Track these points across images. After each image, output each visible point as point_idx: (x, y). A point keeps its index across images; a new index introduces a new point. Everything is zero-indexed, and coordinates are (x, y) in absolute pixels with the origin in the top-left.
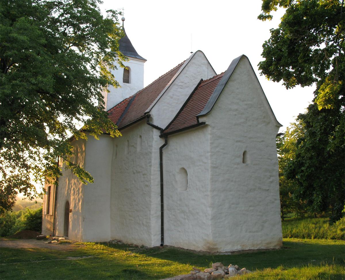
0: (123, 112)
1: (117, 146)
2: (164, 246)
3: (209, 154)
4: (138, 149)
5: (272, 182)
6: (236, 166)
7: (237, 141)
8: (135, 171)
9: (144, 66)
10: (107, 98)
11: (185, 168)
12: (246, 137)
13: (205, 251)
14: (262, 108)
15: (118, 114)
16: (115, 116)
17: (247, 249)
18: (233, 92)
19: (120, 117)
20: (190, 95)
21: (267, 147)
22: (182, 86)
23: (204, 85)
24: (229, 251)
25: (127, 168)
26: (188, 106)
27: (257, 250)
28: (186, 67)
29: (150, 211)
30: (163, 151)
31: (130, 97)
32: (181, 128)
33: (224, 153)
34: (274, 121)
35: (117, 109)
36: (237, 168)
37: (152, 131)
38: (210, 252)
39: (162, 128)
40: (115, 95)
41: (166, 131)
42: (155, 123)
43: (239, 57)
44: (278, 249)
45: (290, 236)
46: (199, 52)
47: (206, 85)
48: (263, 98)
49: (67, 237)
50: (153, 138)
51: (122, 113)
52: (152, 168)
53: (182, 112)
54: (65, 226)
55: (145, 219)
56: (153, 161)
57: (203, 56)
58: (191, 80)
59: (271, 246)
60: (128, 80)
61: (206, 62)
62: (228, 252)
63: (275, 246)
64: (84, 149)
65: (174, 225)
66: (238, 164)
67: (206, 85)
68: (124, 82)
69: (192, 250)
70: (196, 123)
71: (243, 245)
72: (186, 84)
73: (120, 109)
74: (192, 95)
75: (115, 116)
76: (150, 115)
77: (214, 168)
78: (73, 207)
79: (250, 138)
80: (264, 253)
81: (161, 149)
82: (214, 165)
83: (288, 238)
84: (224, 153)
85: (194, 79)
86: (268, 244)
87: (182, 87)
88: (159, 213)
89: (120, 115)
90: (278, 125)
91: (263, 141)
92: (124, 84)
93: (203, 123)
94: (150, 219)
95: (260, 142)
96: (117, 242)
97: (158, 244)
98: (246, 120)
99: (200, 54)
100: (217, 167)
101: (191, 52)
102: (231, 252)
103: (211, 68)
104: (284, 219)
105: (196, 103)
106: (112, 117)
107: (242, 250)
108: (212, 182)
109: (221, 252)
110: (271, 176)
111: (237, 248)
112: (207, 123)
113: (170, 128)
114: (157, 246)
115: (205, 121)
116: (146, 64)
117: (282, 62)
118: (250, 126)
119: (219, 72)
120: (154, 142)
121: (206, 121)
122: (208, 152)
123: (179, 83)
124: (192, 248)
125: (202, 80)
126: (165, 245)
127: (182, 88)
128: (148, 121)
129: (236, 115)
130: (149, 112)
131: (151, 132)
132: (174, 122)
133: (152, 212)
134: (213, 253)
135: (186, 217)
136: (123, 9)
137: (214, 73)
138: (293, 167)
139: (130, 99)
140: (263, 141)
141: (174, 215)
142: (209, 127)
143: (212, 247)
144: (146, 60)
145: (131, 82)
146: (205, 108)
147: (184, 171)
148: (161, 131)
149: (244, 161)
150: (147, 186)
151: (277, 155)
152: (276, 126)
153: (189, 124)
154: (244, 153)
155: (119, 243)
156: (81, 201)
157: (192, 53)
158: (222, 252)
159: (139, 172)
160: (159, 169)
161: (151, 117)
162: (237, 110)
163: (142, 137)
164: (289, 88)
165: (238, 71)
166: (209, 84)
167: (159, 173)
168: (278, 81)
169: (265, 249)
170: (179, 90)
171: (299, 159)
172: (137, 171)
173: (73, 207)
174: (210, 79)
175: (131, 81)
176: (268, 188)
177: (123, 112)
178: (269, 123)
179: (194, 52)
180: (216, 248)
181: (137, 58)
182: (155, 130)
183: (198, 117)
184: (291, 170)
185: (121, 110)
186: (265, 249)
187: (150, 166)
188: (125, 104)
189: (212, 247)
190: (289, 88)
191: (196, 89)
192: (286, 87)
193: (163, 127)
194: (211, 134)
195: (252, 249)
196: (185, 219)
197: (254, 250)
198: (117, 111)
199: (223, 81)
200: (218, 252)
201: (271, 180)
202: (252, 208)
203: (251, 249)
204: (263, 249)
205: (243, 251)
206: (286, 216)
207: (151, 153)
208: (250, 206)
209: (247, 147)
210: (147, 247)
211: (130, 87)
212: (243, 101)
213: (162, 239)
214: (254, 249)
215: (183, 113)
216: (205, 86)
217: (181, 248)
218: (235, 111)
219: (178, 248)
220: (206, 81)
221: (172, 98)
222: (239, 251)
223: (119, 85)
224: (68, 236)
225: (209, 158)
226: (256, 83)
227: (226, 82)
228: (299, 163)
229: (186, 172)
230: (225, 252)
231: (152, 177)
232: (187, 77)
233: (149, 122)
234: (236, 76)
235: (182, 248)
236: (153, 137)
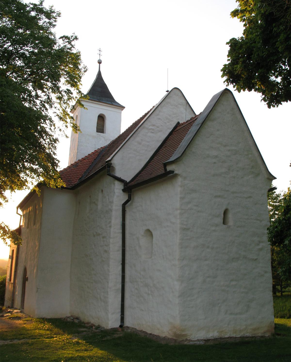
0: (91, 164)
1: (79, 203)
2: (124, 327)
3: (179, 211)
4: (100, 207)
5: (261, 250)
6: (213, 228)
7: (216, 197)
8: (95, 234)
9: (122, 114)
10: (78, 150)
11: (151, 230)
12: (228, 191)
13: (171, 338)
14: (250, 156)
15: (85, 167)
16: (81, 168)
17: (226, 336)
18: (212, 135)
19: (87, 170)
20: (163, 140)
21: (256, 204)
22: (153, 129)
23: (180, 129)
24: (202, 339)
25: (88, 230)
26: (159, 154)
27: (240, 337)
29: (108, 282)
30: (127, 209)
31: (101, 147)
32: (147, 179)
33: (198, 212)
34: (264, 172)
35: (85, 160)
36: (214, 231)
37: (114, 184)
38: (177, 340)
39: (125, 181)
40: (87, 146)
41: (130, 184)
43: (221, 91)
44: (268, 336)
45: (288, 315)
47: (182, 128)
48: (251, 142)
49: (23, 310)
50: (114, 193)
51: (89, 166)
52: (112, 230)
53: (153, 161)
55: (103, 292)
56: (113, 221)
57: (180, 94)
58: (165, 123)
59: (259, 333)
61: (184, 101)
62: (201, 340)
63: (265, 333)
64: (41, 206)
66: (217, 225)
67: (182, 128)
68: (97, 131)
69: (155, 335)
70: (163, 172)
71: (222, 331)
72: (158, 127)
74: (166, 141)
75: (81, 168)
76: (111, 164)
77: (184, 229)
79: (233, 193)
80: (248, 343)
81: (124, 205)
82: (185, 227)
83: (286, 318)
84: (198, 212)
85: (168, 122)
86: (255, 329)
87: (153, 131)
88: (120, 286)
89: (86, 167)
90: (271, 178)
91: (250, 197)
93: (172, 172)
94: (107, 292)
95: (247, 198)
96: (72, 320)
97: (117, 324)
98: (229, 170)
100: (188, 229)
101: (167, 90)
102: (205, 340)
103: (190, 110)
104: (283, 294)
105: (168, 149)
106: (78, 169)
107: (220, 338)
109: (191, 340)
110: (260, 242)
111: (213, 334)
112: (176, 172)
113: (136, 180)
114: (115, 327)
115: (174, 170)
116: (124, 112)
117: (254, 56)
118: (234, 177)
119: (197, 113)
120: (115, 197)
121: (176, 169)
122: (177, 209)
123: (149, 126)
124: (156, 333)
125: (178, 123)
126: (126, 327)
127: (153, 133)
128: (109, 171)
129: (215, 163)
130: (110, 160)
131: (113, 185)
132: (142, 173)
133: (110, 285)
134: (181, 341)
135: (150, 292)
136: (100, 55)
138: (279, 228)
139: (101, 150)
140: (250, 197)
141: (136, 289)
142: (179, 177)
143: (178, 332)
144: (124, 107)
145: (106, 132)
146: (175, 154)
147: (149, 233)
148: (124, 184)
149: (224, 222)
150: (106, 251)
152: (268, 179)
153: (156, 175)
154: (226, 212)
155: (76, 321)
156: (36, 268)
158: (193, 340)
159: (99, 235)
160: (121, 231)
161: (113, 167)
162: (216, 157)
163: (104, 192)
164: (271, 106)
165: (219, 109)
166: (185, 127)
167: (120, 236)
168: (251, 90)
169: (250, 337)
170: (150, 134)
171: (289, 215)
172: (96, 233)
174: (187, 122)
175: (106, 130)
176: (256, 257)
177: (91, 164)
178: (258, 175)
180: (185, 334)
181: (114, 104)
182: (117, 182)
183: (165, 165)
184: (277, 232)
185: (89, 162)
186: (251, 336)
187: (110, 227)
188: (95, 155)
189: (180, 334)
190: (271, 106)
191: (171, 134)
192: (267, 104)
193: (128, 180)
194: (181, 187)
195: (233, 337)
196: (149, 294)
197: (236, 338)
198: (84, 163)
199: (199, 121)
200: (187, 340)
201: (260, 247)
202: (233, 283)
203: (231, 336)
204: (248, 337)
205: (221, 338)
206: (285, 290)
207: (111, 210)
208: (232, 280)
209: (229, 204)
210: (104, 328)
211: (104, 138)
212: (225, 146)
214: (237, 336)
215: (153, 162)
216: (181, 129)
217: (144, 332)
218: (214, 158)
219: (141, 331)
220: (182, 124)
221: (140, 144)
222: (216, 339)
223: (79, 130)
224: (23, 309)
225: (178, 217)
226: (243, 124)
227: (203, 121)
228: (287, 222)
229: (151, 235)
230: (196, 339)
231: (111, 240)
232: (159, 119)
233: (109, 172)
234: (216, 114)
235: (145, 331)
236: (114, 191)
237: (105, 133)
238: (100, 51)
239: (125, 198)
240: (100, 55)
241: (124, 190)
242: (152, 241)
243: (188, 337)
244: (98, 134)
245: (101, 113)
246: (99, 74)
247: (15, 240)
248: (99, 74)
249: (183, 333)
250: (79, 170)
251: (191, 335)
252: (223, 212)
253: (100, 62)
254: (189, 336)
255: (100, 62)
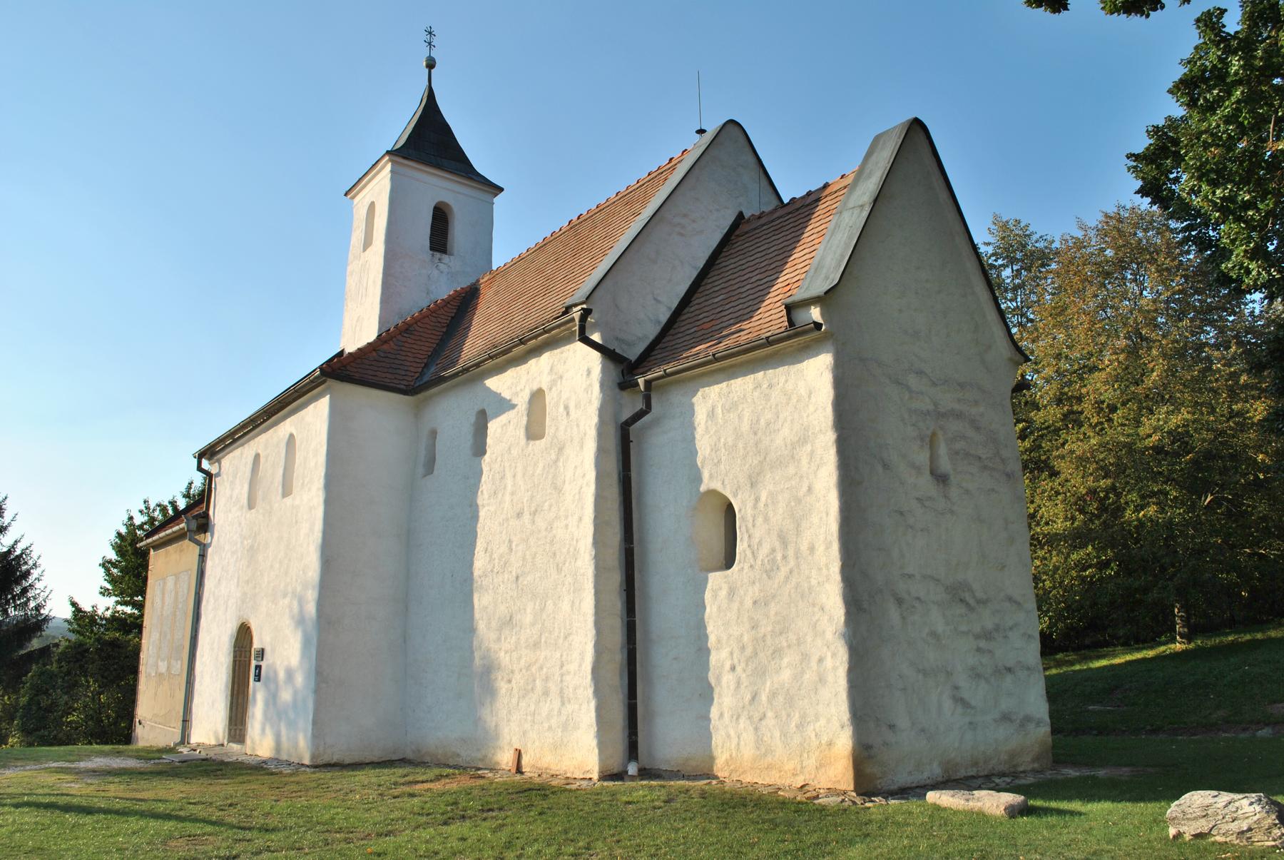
28: (696, 166)
46: (730, 127)
61: (753, 160)
73: (433, 319)
78: (366, 376)
85: (718, 210)
99: (733, 130)
116: (498, 200)
136: (430, 44)
137: (773, 197)
144: (501, 190)
151: (488, 389)
157: (701, 132)
173: (366, 376)
185: (439, 325)
237: (451, 254)
238: (430, 33)
243: (879, 782)
245: (453, 206)
247: (109, 619)
253: (431, 65)
254: (880, 778)
255: (431, 65)
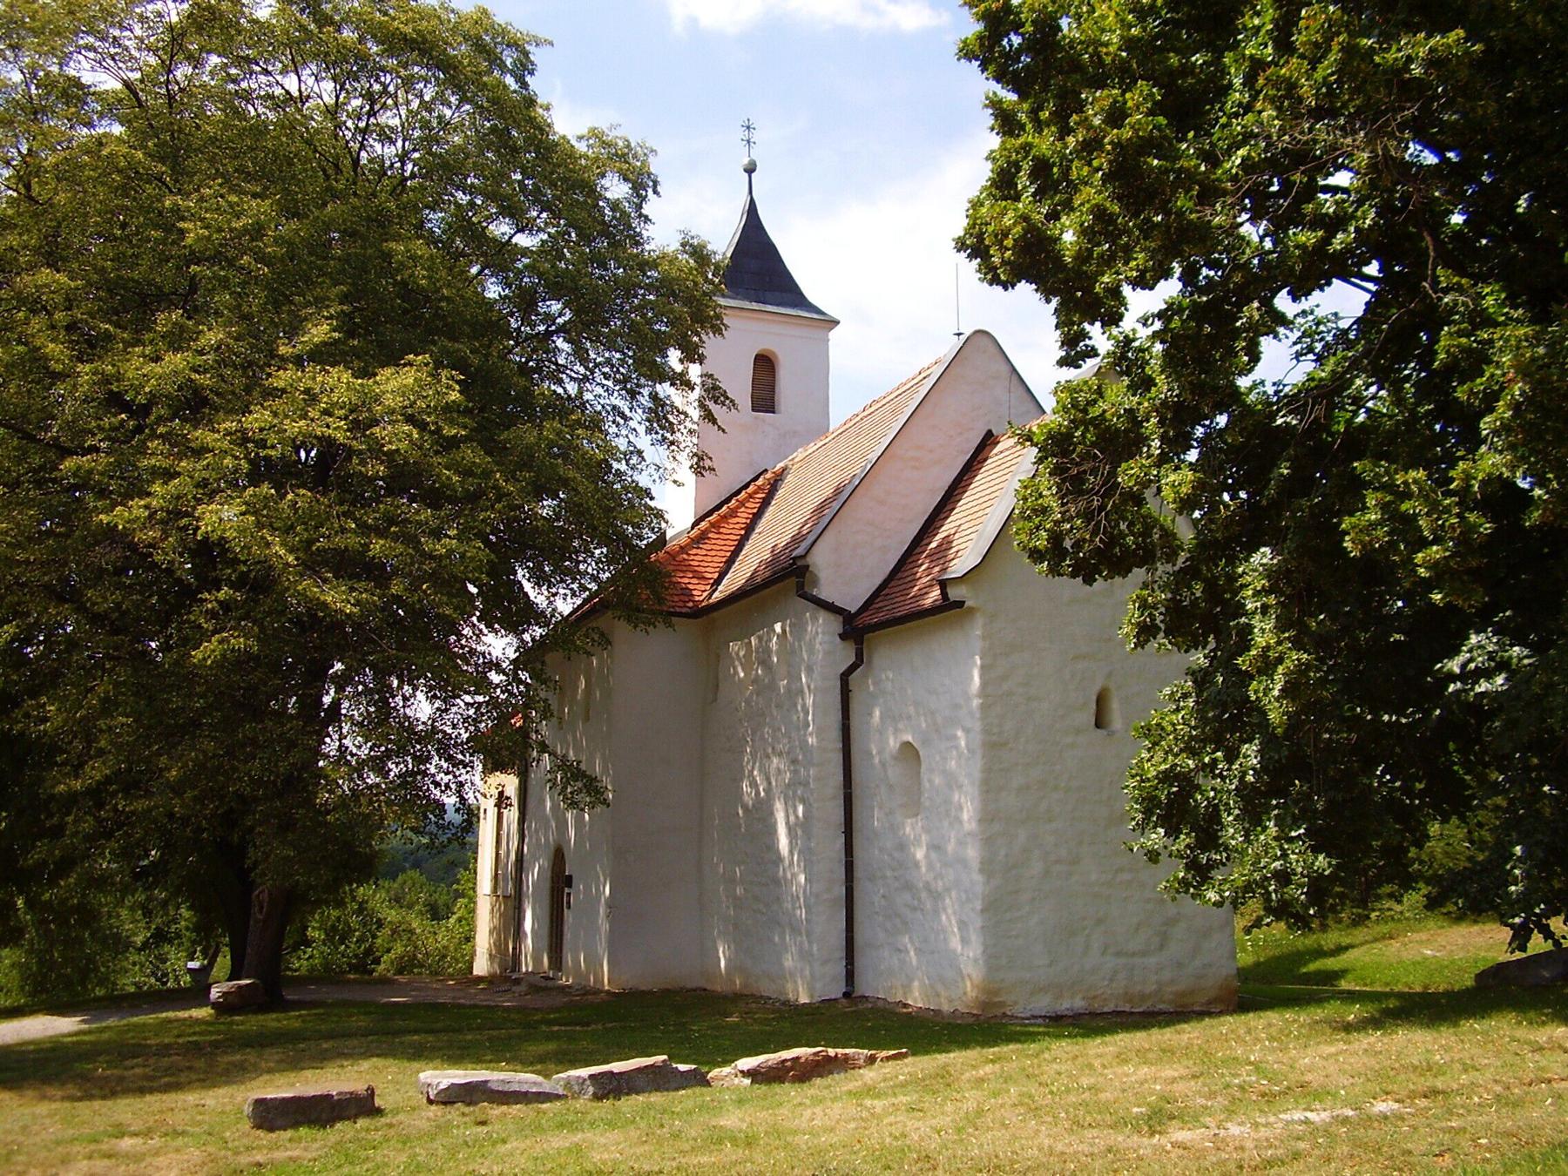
42: (825, 592)
54: (551, 935)
60: (772, 400)
65: (886, 931)
66: (1078, 731)
71: (1095, 997)
72: (931, 451)
81: (845, 677)
82: (994, 738)
92: (756, 418)
103: (1021, 390)
108: (987, 792)
116: (834, 335)
130: (803, 557)
136: (748, 142)
141: (883, 896)
142: (978, 615)
144: (837, 323)
149: (1100, 723)
154: (1101, 701)
167: (838, 758)
175: (782, 400)
179: (968, 333)
182: (823, 617)
202: (1126, 876)
208: (1121, 870)
213: (850, 976)
230: (1028, 1015)
239: (846, 656)
240: (748, 142)
241: (843, 637)
242: (919, 773)
244: (756, 418)
246: (752, 211)
248: (752, 211)
249: (997, 1000)
250: (713, 553)
251: (1016, 1003)
252: (1094, 698)
253: (750, 170)
255: (750, 170)
